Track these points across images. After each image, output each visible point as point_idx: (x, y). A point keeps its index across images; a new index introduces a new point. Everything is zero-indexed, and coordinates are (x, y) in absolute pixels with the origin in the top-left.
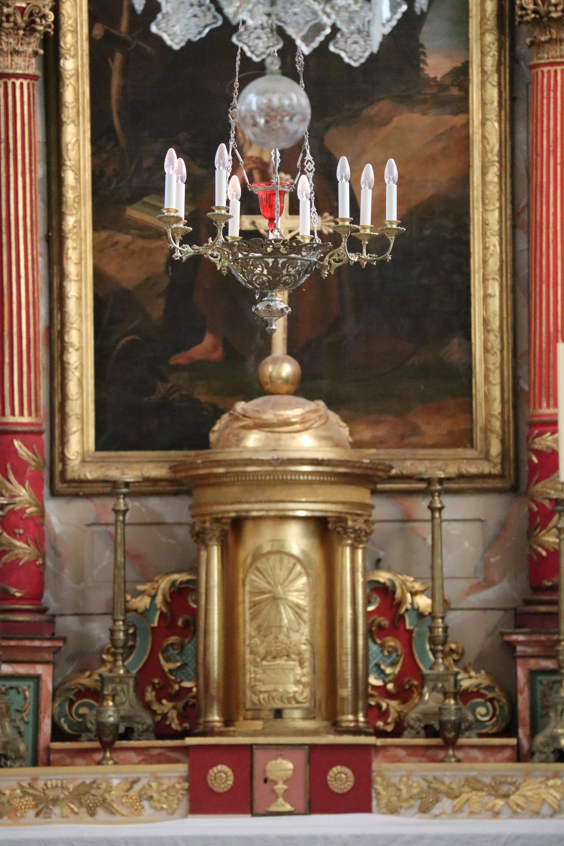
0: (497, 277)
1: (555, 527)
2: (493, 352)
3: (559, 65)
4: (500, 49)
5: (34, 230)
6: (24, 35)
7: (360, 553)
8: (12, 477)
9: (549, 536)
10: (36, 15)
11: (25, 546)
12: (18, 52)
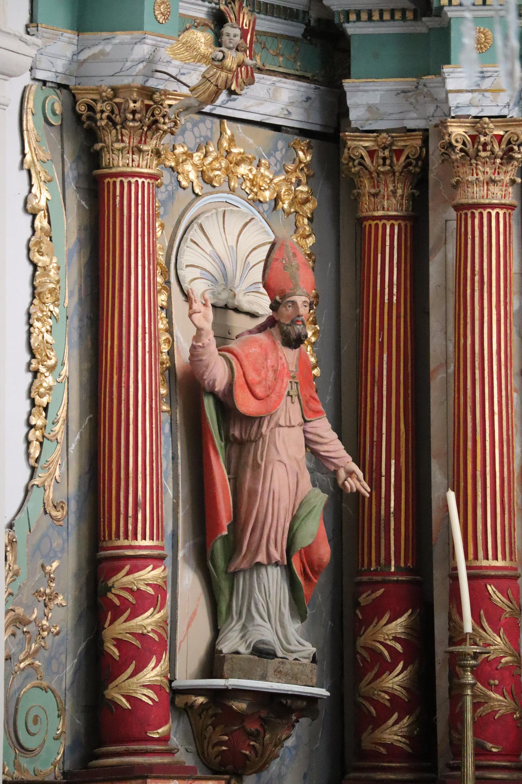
5: (509, 365)
6: (501, 164)
7: (150, 703)
8: (486, 624)
10: (514, 143)
11: (501, 698)
12: (494, 182)
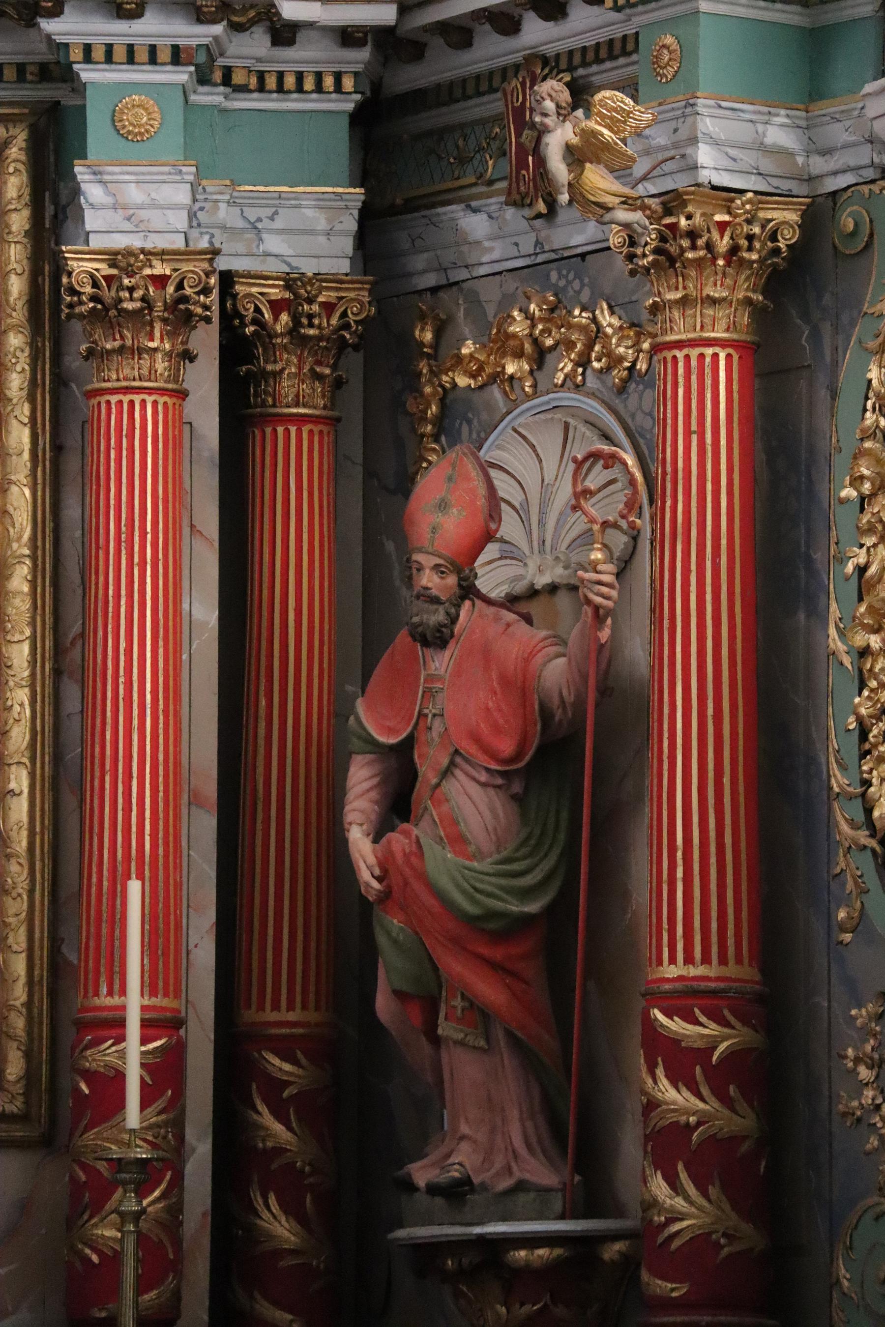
0: (25, 760)
1: (116, 1211)
2: (14, 894)
3: (138, 393)
4: (35, 358)
9: (105, 1227)
